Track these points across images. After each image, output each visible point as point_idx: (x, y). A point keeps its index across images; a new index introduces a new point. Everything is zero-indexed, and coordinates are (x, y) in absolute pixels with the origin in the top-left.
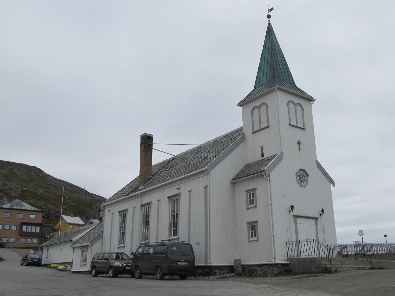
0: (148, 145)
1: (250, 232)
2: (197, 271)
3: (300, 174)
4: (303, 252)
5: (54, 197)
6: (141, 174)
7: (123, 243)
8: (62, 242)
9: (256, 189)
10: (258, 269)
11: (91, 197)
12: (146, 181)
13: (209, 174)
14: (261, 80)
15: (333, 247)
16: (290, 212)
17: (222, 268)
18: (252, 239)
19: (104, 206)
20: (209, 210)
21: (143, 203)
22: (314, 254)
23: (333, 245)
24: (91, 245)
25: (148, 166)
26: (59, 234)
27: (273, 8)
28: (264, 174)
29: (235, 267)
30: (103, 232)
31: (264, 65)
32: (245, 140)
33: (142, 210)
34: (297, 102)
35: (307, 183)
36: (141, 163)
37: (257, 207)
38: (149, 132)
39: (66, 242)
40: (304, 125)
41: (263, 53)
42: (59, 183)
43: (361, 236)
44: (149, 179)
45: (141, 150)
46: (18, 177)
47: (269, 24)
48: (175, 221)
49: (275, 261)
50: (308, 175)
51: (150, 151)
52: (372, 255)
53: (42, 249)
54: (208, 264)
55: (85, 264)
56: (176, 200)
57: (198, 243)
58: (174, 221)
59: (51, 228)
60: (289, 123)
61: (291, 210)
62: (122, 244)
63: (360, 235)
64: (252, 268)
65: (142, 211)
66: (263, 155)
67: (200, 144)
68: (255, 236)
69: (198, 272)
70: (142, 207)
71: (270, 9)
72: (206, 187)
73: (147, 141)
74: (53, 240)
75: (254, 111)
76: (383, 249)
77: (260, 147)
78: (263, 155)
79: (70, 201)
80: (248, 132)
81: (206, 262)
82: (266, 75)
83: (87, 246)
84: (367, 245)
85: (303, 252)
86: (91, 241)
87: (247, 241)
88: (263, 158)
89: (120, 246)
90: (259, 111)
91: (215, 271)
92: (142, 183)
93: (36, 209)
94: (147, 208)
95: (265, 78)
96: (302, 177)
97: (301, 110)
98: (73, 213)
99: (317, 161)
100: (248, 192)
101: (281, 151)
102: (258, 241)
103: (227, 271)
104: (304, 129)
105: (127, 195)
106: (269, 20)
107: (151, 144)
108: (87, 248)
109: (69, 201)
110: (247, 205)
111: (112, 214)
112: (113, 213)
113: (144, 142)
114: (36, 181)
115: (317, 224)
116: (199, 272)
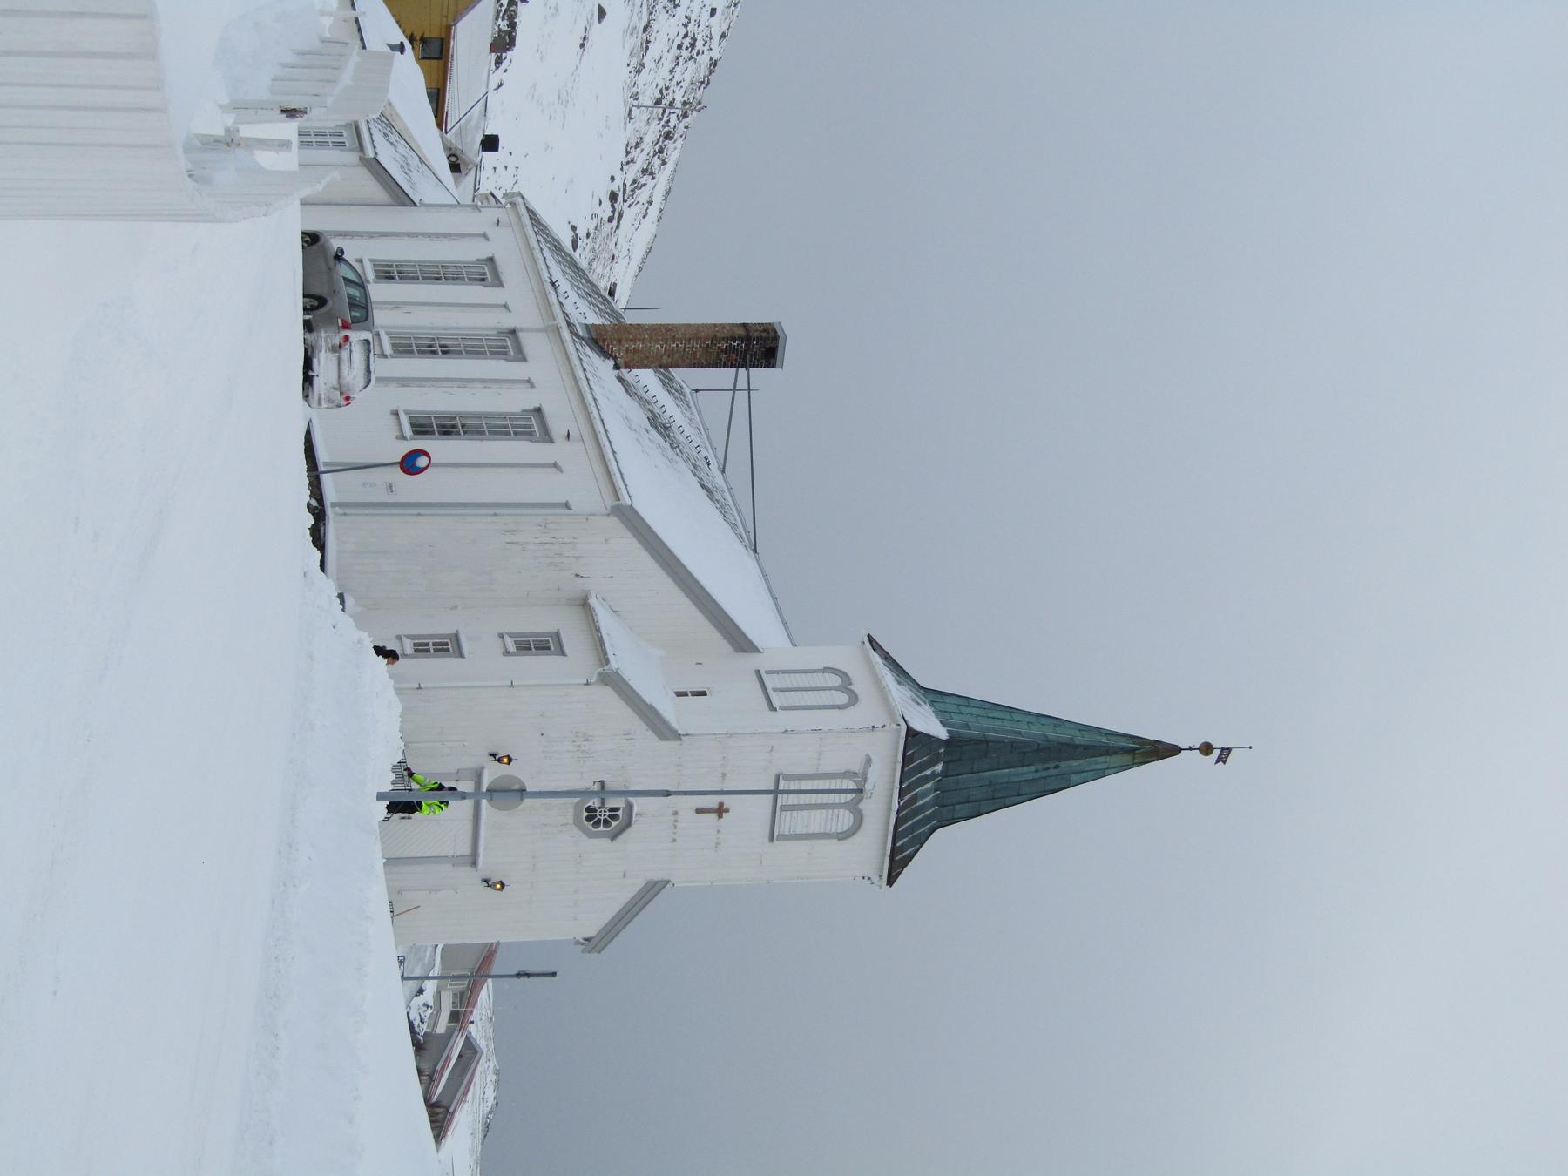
9: (563, 654)
13: (608, 515)
16: (491, 755)
35: (591, 835)
36: (674, 329)
37: (505, 658)
38: (791, 351)
39: (356, 29)
40: (783, 837)
47: (1174, 750)
50: (614, 837)
57: (391, 487)
61: (497, 758)
70: (509, 333)
100: (454, 640)
101: (687, 735)
106: (1190, 749)
107: (745, 361)
110: (511, 635)
112: (488, 240)
115: (455, 860)
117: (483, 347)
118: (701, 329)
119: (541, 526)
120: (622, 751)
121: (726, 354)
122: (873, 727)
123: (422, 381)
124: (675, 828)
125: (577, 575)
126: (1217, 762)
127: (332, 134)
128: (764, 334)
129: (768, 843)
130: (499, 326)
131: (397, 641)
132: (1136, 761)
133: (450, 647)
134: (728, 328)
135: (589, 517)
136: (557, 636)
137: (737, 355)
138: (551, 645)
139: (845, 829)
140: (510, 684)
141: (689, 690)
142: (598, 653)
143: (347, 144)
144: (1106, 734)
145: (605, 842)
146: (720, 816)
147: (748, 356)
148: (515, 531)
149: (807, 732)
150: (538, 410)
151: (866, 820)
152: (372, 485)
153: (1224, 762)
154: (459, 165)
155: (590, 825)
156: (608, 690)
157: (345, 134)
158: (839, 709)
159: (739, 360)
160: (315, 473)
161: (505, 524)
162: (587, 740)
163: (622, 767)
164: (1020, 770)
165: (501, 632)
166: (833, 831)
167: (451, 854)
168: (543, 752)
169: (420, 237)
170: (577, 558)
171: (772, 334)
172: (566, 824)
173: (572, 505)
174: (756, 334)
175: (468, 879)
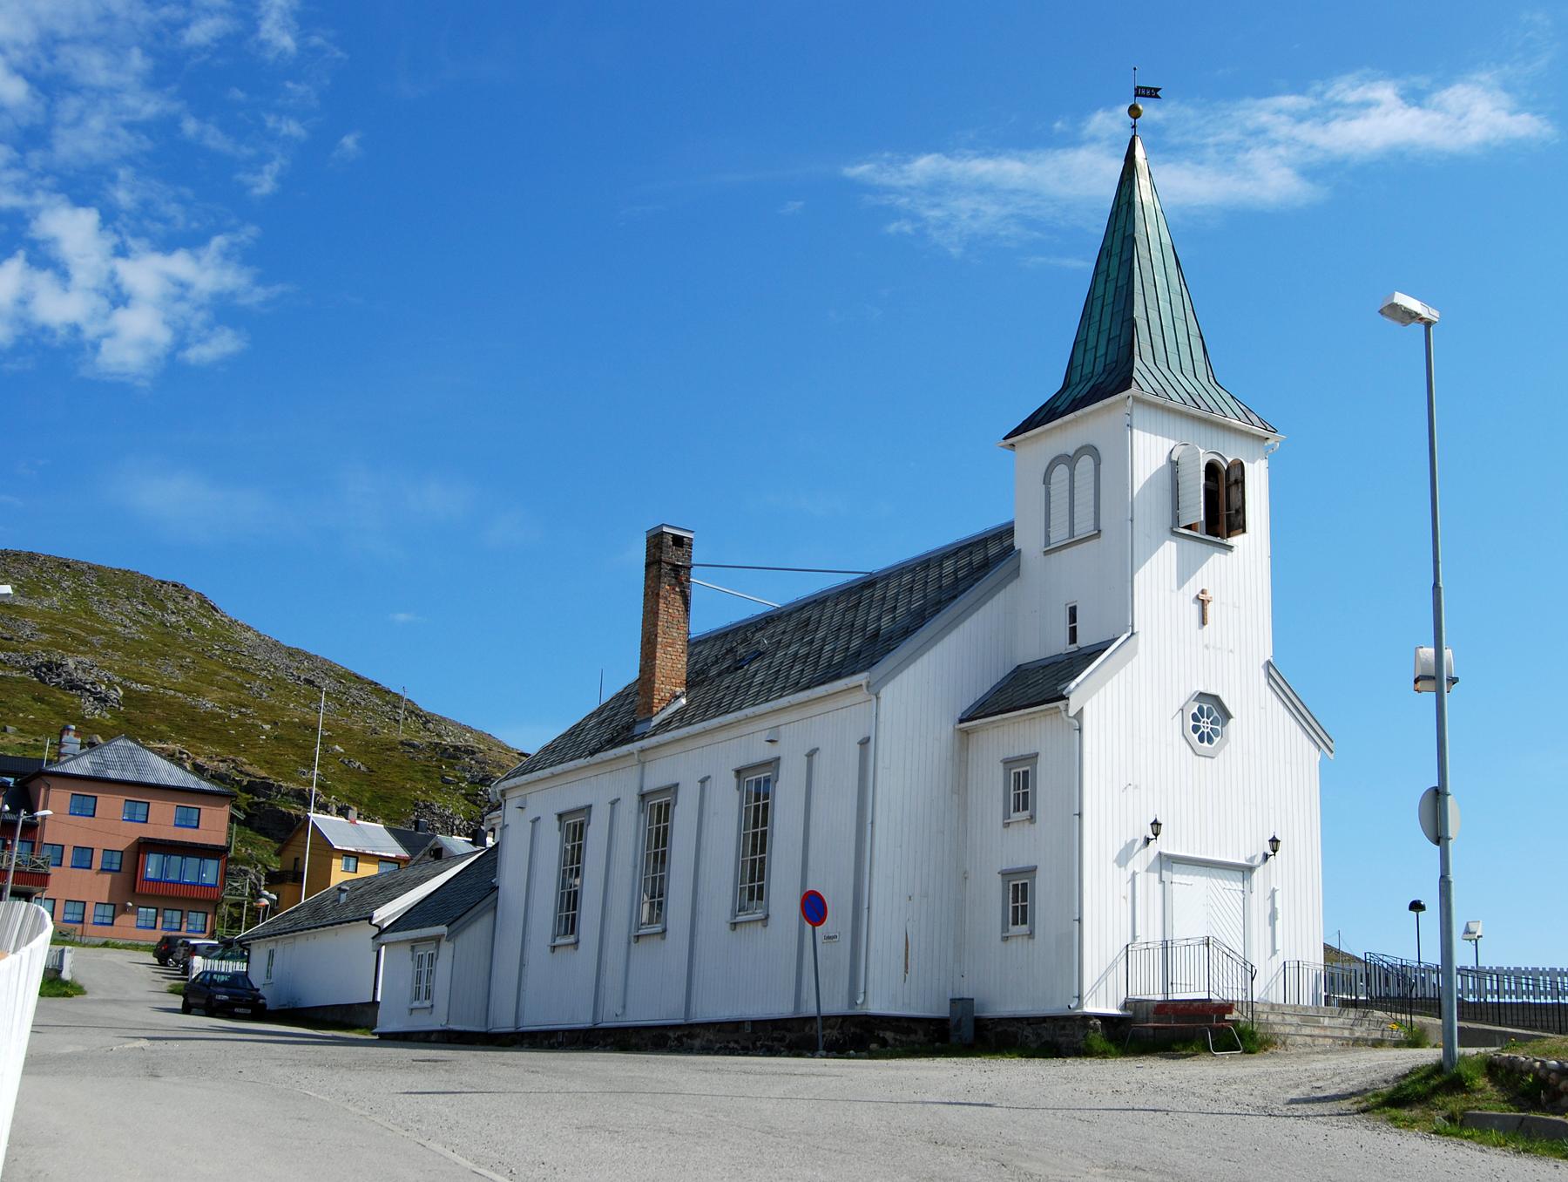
1: (1011, 905)
3: (1200, 710)
4: (1179, 982)
5: (267, 727)
6: (646, 676)
7: (572, 933)
8: (332, 925)
10: (1025, 1033)
14: (1090, 356)
15: (1301, 969)
16: (1148, 843)
18: (1014, 930)
19: (503, 792)
20: (872, 823)
22: (1207, 989)
26: (303, 901)
28: (1062, 708)
29: (952, 1024)
31: (1104, 299)
32: (1019, 575)
33: (643, 811)
42: (288, 662)
43: (1474, 942)
46: (105, 633)
48: (660, 850)
49: (1080, 1005)
52: (1490, 1011)
53: (246, 947)
54: (859, 1011)
55: (427, 1003)
56: (765, 781)
57: (829, 938)
58: (752, 858)
59: (260, 866)
62: (566, 933)
63: (1470, 941)
64: (1010, 1029)
66: (1073, 639)
67: (870, 571)
68: (1024, 922)
74: (291, 916)
76: (1489, 987)
77: (1066, 605)
79: (342, 750)
81: (852, 1001)
84: (1431, 972)
85: (1179, 982)
86: (451, 919)
87: (1000, 937)
88: (1073, 648)
89: (559, 941)
90: (1072, 476)
91: (881, 1035)
93: (205, 785)
94: (660, 807)
95: (1101, 351)
96: (1205, 719)
98: (359, 804)
103: (925, 1036)
106: (1134, 127)
108: (438, 947)
114: (188, 654)
117: (658, 829)
118: (649, 608)
126: (1157, 97)
127: (420, 966)
130: (635, 811)
131: (1009, 941)
133: (1020, 882)
134: (650, 582)
136: (1008, 763)
144: (1118, 207)
150: (738, 772)
153: (1158, 90)
154: (437, 849)
157: (421, 953)
160: (819, 1021)
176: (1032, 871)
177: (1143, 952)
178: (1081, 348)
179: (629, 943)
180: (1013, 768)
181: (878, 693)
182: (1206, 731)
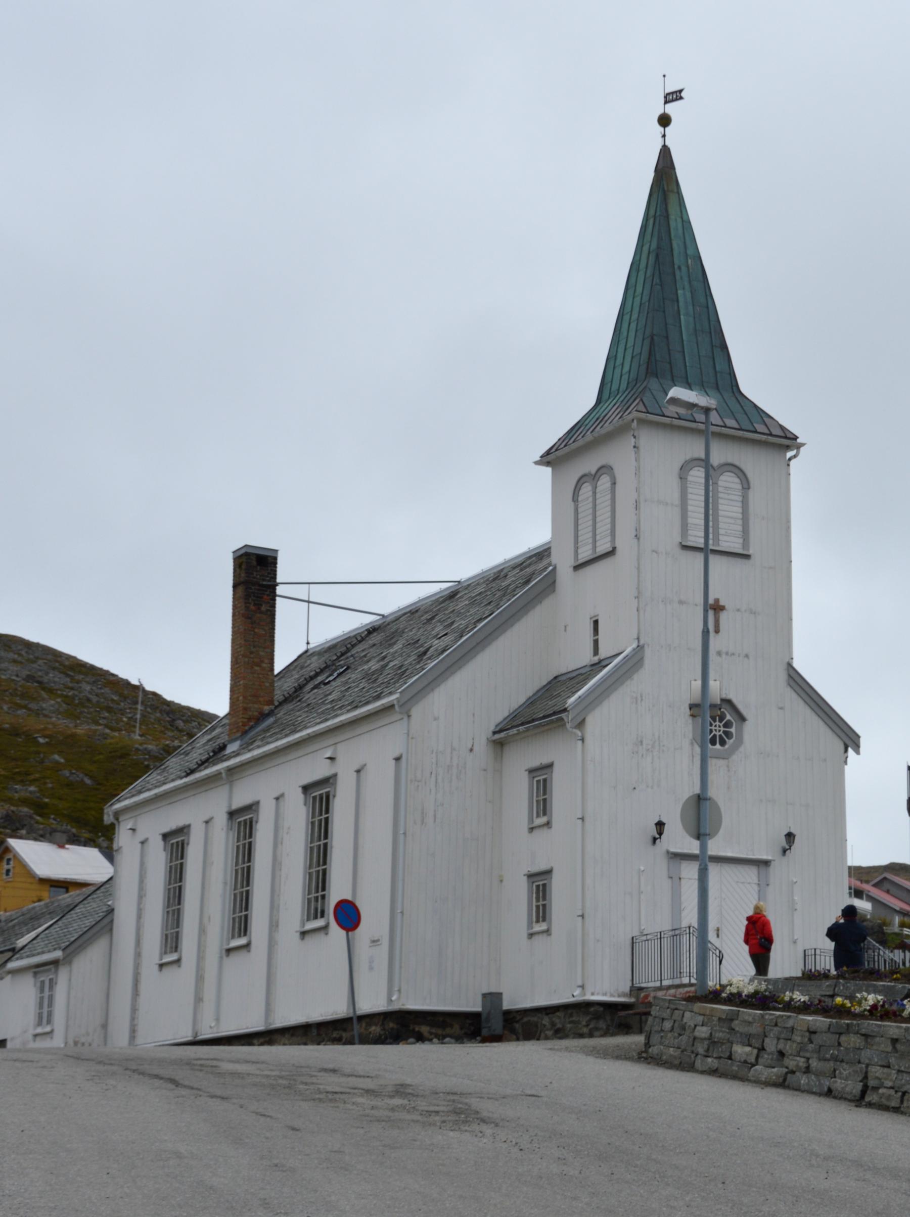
0: (257, 587)
1: (534, 903)
2: (370, 1030)
4: (685, 970)
9: (550, 766)
11: (181, 731)
12: (252, 724)
13: (409, 716)
15: (818, 957)
17: (441, 1019)
19: (117, 815)
21: (237, 804)
23: (818, 952)
24: (67, 960)
25: (257, 668)
27: (681, 91)
29: (484, 1017)
30: (111, 911)
33: (231, 829)
34: (723, 461)
35: (740, 741)
38: (261, 541)
41: (635, 266)
44: (263, 716)
45: (235, 607)
47: (665, 154)
50: (743, 719)
51: (268, 610)
55: (48, 1029)
57: (374, 941)
60: (679, 540)
61: (657, 836)
65: (231, 833)
67: (458, 580)
68: (544, 920)
69: (370, 1033)
71: (672, 93)
72: (398, 759)
73: (255, 573)
75: (581, 492)
78: (596, 651)
80: (562, 560)
82: (631, 356)
83: (55, 963)
88: (596, 659)
90: (594, 493)
91: (417, 1029)
92: (238, 731)
95: (626, 368)
97: (740, 487)
99: (790, 666)
100: (535, 774)
101: (638, 639)
102: (550, 935)
103: (461, 1029)
104: (747, 557)
105: (188, 775)
106: (664, 136)
109: (56, 757)
110: (531, 820)
111: (142, 843)
112: (282, 795)
113: (242, 580)
116: (372, 1032)
119: (418, 786)
120: (654, 706)
121: (261, 605)
122: (635, 447)
123: (274, 907)
124: (733, 654)
125: (471, 750)
127: (42, 990)
128: (244, 567)
129: (751, 561)
130: (225, 829)
131: (533, 938)
132: (676, 190)
133: (541, 883)
135: (410, 736)
137: (263, 594)
138: (541, 778)
139: (737, 480)
140: (581, 820)
141: (592, 638)
142: (550, 729)
143: (51, 977)
145: (748, 727)
146: (722, 608)
147: (265, 583)
148: (423, 813)
149: (638, 515)
151: (730, 460)
152: (371, 961)
155: (730, 742)
156: (590, 720)
157: (42, 979)
158: (615, 483)
159: (268, 593)
160: (355, 1021)
161: (415, 823)
162: (641, 742)
163: (670, 706)
164: (681, 304)
165: (525, 935)
166: (740, 494)
167: (756, 888)
168: (652, 788)
169: (142, 906)
170: (453, 749)
171: (244, 559)
172: (728, 766)
173: (396, 755)
174: (243, 575)
175: (780, 870)
176: (548, 872)
177: (643, 943)
178: (612, 363)
179: (221, 958)
180: (536, 777)
181: (410, 710)
182: (718, 734)
